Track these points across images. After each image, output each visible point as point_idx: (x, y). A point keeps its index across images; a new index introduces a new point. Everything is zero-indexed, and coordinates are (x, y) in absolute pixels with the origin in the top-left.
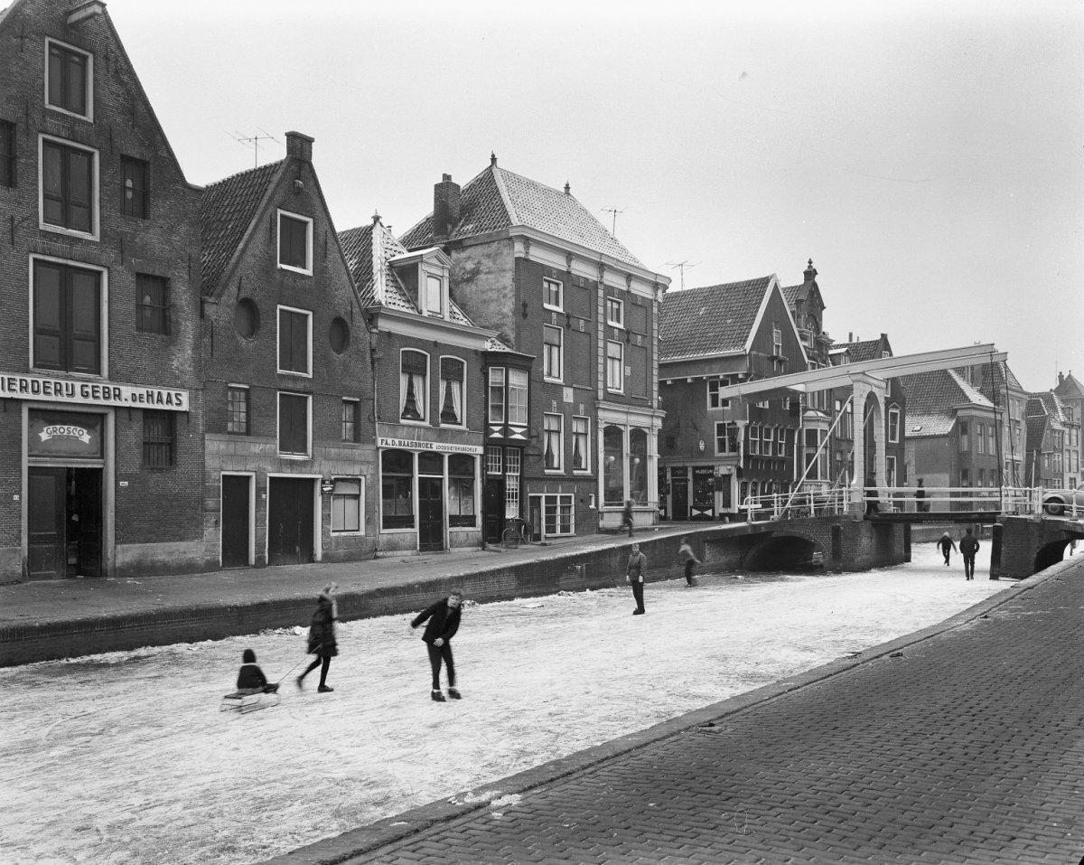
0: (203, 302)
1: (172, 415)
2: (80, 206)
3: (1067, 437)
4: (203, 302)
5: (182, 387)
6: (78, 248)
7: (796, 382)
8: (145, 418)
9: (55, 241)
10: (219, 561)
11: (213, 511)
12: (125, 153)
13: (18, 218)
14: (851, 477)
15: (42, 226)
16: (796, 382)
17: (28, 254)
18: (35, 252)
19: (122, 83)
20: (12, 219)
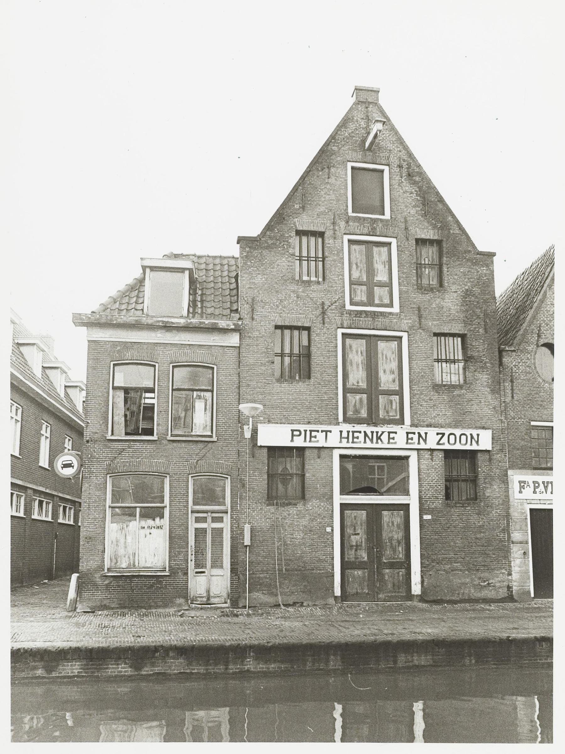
0: (501, 352)
1: (473, 454)
2: (362, 285)
3: (467, 472)
4: (501, 352)
5: (141, 397)
6: (380, 321)
7: (279, 596)
8: (446, 457)
9: (359, 317)
10: (529, 592)
11: (521, 543)
12: (419, 237)
13: (327, 303)
14: (355, 405)
15: (348, 307)
16: (279, 596)
17: (336, 330)
18: (342, 327)
19: (415, 183)
20: (323, 304)
